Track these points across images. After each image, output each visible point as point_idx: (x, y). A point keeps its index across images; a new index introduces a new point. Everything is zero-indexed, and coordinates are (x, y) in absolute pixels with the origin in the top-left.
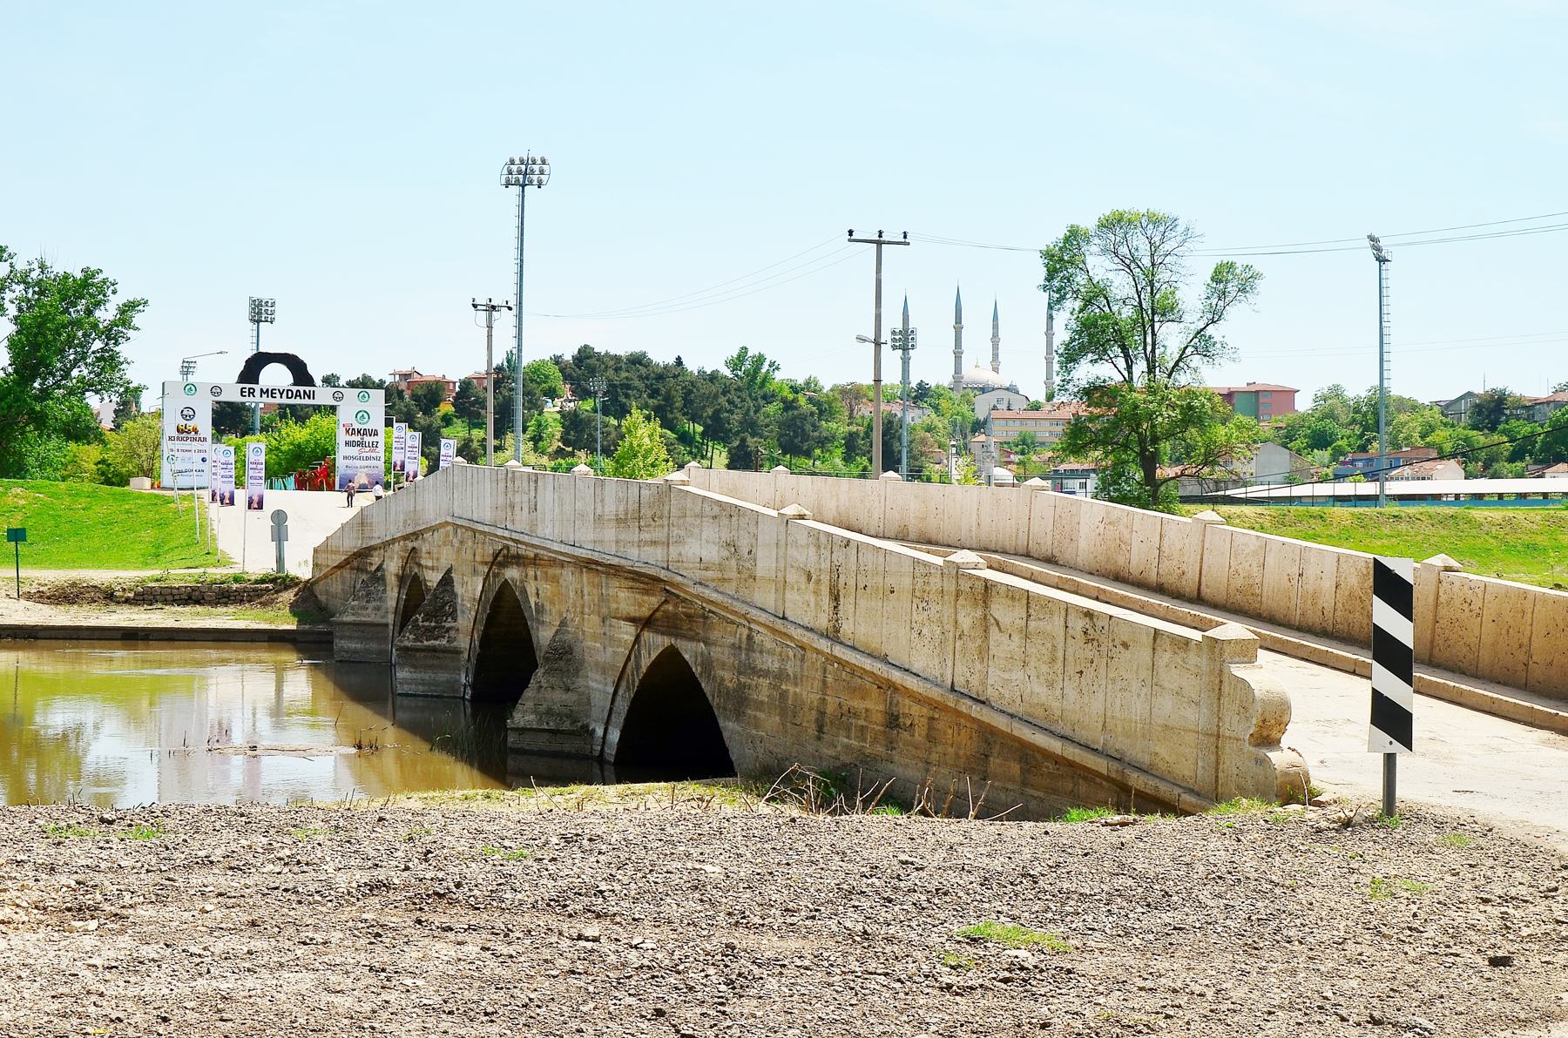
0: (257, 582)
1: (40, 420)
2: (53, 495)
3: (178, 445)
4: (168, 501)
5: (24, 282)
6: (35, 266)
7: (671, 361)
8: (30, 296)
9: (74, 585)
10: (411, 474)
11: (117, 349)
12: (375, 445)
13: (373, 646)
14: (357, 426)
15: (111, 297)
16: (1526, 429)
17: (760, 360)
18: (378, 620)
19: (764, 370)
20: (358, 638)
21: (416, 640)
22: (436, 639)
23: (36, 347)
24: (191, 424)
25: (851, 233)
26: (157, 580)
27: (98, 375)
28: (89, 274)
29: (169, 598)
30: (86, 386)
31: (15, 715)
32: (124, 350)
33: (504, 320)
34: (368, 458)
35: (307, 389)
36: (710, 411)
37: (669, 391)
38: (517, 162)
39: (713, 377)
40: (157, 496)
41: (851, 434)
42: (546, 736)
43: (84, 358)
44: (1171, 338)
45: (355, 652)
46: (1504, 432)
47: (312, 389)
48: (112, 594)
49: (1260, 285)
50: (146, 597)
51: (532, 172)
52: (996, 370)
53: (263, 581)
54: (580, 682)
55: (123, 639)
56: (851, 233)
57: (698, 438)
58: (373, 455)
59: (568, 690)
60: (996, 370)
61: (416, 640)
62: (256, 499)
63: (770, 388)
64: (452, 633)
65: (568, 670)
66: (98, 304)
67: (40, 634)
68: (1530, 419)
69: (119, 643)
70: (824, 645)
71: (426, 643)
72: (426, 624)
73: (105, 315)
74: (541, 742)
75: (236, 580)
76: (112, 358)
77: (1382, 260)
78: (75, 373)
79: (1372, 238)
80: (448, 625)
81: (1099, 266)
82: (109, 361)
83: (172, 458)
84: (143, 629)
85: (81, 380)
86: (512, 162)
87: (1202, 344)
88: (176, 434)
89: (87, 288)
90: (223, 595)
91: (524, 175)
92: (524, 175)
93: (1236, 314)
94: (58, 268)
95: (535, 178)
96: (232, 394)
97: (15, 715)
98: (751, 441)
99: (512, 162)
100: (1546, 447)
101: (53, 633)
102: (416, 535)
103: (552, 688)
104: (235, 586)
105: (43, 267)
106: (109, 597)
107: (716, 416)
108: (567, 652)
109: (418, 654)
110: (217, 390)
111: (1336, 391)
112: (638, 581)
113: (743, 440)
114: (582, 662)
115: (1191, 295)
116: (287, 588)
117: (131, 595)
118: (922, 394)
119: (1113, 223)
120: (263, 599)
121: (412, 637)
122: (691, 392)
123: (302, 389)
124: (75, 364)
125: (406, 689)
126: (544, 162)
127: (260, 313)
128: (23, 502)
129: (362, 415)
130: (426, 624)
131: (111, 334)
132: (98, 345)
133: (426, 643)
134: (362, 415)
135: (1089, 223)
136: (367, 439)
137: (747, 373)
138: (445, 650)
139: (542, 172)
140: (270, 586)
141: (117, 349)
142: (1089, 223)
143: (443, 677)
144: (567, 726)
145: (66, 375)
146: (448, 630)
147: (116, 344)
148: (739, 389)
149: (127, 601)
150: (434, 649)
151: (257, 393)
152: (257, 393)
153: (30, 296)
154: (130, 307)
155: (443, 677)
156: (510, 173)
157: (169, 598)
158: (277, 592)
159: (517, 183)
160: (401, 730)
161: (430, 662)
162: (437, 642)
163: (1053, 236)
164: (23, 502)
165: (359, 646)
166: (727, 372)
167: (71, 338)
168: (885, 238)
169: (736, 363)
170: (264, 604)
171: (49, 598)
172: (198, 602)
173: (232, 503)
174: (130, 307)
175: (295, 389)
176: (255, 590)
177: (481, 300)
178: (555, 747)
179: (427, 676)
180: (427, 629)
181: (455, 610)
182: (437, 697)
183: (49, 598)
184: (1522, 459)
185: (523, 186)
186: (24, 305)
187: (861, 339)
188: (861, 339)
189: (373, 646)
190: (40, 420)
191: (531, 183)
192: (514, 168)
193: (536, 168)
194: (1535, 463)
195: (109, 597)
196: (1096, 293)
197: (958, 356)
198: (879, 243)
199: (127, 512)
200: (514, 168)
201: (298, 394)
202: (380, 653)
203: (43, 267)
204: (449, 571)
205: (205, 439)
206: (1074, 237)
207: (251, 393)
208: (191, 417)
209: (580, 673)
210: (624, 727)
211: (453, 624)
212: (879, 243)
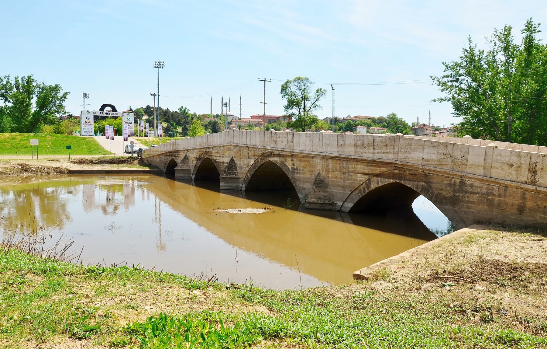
0: (127, 158)
1: (45, 120)
2: (58, 137)
3: (86, 125)
4: (86, 139)
5: (39, 87)
6: (42, 83)
7: (166, 109)
8: (40, 90)
9: (82, 159)
11: (62, 103)
12: (132, 126)
13: (186, 175)
14: (127, 121)
15: (61, 91)
16: (341, 125)
17: (185, 109)
18: (188, 169)
19: (186, 111)
20: (182, 173)
21: (226, 175)
22: (232, 175)
23: (44, 102)
25: (259, 78)
26: (103, 158)
27: (58, 109)
28: (56, 85)
29: (107, 162)
30: (55, 112)
32: (64, 104)
33: (156, 97)
34: (130, 129)
35: (116, 113)
36: (177, 119)
37: (168, 115)
38: (157, 62)
39: (176, 112)
40: (83, 137)
41: (206, 124)
42: (319, 205)
43: (55, 105)
44: (308, 104)
45: (181, 176)
46: (337, 125)
48: (92, 162)
50: (101, 162)
51: (161, 65)
52: (230, 111)
53: (129, 158)
54: (329, 190)
55: (105, 173)
56: (259, 78)
57: (175, 125)
59: (325, 192)
60: (230, 111)
61: (226, 175)
62: (126, 138)
63: (188, 115)
64: (236, 174)
65: (324, 187)
66: (58, 93)
67: (84, 172)
68: (342, 122)
69: (104, 174)
70: (530, 187)
71: (229, 176)
72: (228, 171)
73: (60, 95)
74: (317, 206)
75: (122, 158)
76: (62, 105)
77: (333, 90)
78: (53, 109)
79: (331, 85)
80: (235, 171)
81: (293, 88)
82: (60, 106)
83: (84, 129)
84: (111, 171)
85: (54, 110)
86: (156, 62)
87: (315, 106)
89: (55, 89)
90: (113, 162)
91: (159, 65)
92: (159, 65)
93: (322, 99)
94: (47, 84)
95: (162, 66)
96: (98, 114)
98: (187, 126)
99: (156, 62)
100: (345, 128)
101: (87, 172)
103: (319, 191)
104: (122, 159)
105: (43, 84)
106: (91, 162)
107: (179, 120)
108: (322, 182)
109: (227, 179)
110: (94, 112)
111: (394, 115)
112: (369, 163)
113: (185, 126)
114: (328, 184)
115: (311, 94)
116: (135, 160)
117: (97, 162)
118: (217, 116)
119: (297, 79)
120: (130, 162)
121: (224, 174)
122: (173, 115)
123: (114, 113)
124: (53, 107)
125: (223, 188)
126: (163, 63)
127: (85, 96)
128: (50, 139)
129: (129, 119)
130: (228, 171)
131: (61, 100)
132: (58, 102)
133: (229, 176)
134: (129, 119)
135: (292, 79)
136: (130, 124)
137: (183, 111)
138: (235, 178)
139: (163, 65)
140: (131, 159)
141: (62, 103)
142: (292, 79)
143: (234, 185)
144: (327, 202)
145: (51, 109)
146: (235, 173)
147: (63, 102)
148: (181, 115)
149: (96, 163)
150: (232, 178)
151: (104, 114)
152: (104, 114)
153: (40, 90)
155: (234, 185)
156: (156, 65)
157: (107, 162)
158: (133, 161)
159: (157, 67)
161: (230, 181)
162: (232, 176)
163: (283, 82)
164: (50, 139)
165: (182, 175)
166: (179, 111)
167: (52, 100)
168: (266, 80)
169: (181, 109)
170: (131, 163)
171: (77, 163)
172: (113, 163)
173: (108, 138)
175: (113, 113)
176: (127, 160)
178: (322, 208)
179: (229, 185)
180: (229, 172)
181: (236, 168)
182: (233, 190)
183: (77, 163)
184: (341, 130)
185: (159, 68)
186: (39, 93)
187: (261, 103)
188: (261, 103)
189: (186, 175)
190: (45, 120)
191: (160, 67)
192: (157, 64)
193: (162, 64)
194: (343, 131)
195: (91, 162)
196: (293, 94)
197: (211, 109)
198: (265, 81)
199: (77, 141)
200: (157, 64)
202: (188, 177)
203: (43, 84)
204: (233, 157)
206: (288, 82)
207: (103, 113)
208: (89, 119)
209: (328, 187)
210: (356, 203)
211: (236, 171)
212: (265, 81)
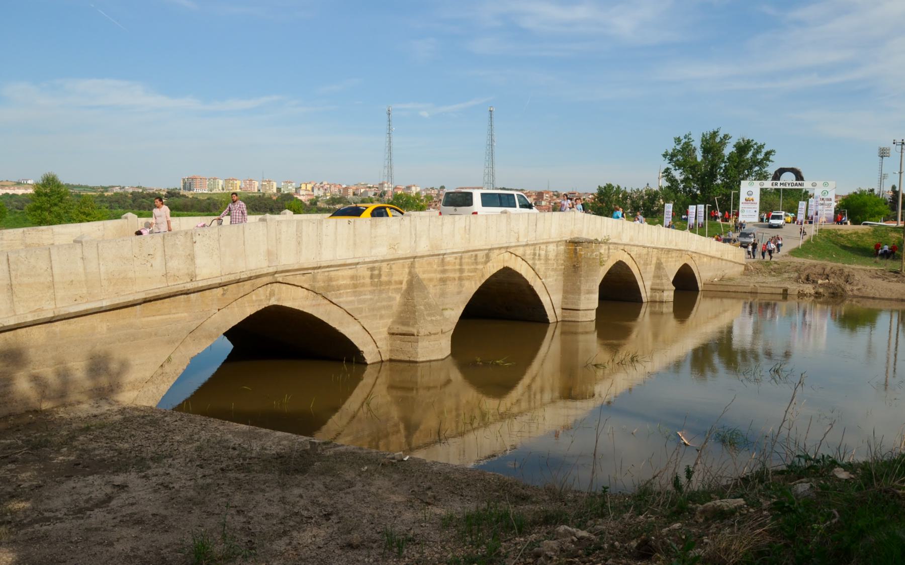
3: (746, 206)
10: (800, 221)
24: (751, 197)
31: (576, 333)
35: (800, 182)
47: (802, 182)
49: (882, 147)
58: (829, 209)
88: (745, 201)
97: (576, 333)
102: (415, 258)
123: (798, 182)
136: (827, 202)
151: (779, 184)
154: (768, 154)
160: (67, 312)
174: (768, 154)
177: (904, 141)
201: (796, 184)
205: (756, 203)
208: (751, 195)
